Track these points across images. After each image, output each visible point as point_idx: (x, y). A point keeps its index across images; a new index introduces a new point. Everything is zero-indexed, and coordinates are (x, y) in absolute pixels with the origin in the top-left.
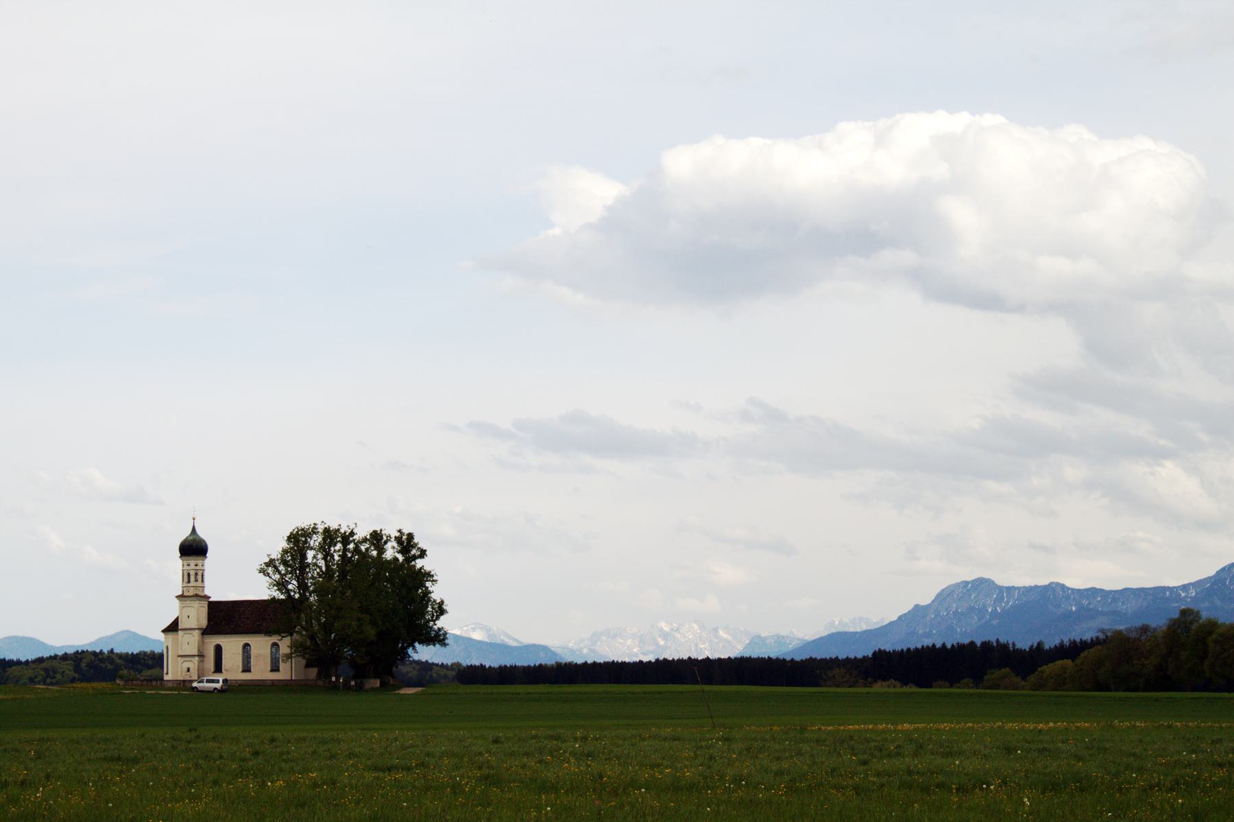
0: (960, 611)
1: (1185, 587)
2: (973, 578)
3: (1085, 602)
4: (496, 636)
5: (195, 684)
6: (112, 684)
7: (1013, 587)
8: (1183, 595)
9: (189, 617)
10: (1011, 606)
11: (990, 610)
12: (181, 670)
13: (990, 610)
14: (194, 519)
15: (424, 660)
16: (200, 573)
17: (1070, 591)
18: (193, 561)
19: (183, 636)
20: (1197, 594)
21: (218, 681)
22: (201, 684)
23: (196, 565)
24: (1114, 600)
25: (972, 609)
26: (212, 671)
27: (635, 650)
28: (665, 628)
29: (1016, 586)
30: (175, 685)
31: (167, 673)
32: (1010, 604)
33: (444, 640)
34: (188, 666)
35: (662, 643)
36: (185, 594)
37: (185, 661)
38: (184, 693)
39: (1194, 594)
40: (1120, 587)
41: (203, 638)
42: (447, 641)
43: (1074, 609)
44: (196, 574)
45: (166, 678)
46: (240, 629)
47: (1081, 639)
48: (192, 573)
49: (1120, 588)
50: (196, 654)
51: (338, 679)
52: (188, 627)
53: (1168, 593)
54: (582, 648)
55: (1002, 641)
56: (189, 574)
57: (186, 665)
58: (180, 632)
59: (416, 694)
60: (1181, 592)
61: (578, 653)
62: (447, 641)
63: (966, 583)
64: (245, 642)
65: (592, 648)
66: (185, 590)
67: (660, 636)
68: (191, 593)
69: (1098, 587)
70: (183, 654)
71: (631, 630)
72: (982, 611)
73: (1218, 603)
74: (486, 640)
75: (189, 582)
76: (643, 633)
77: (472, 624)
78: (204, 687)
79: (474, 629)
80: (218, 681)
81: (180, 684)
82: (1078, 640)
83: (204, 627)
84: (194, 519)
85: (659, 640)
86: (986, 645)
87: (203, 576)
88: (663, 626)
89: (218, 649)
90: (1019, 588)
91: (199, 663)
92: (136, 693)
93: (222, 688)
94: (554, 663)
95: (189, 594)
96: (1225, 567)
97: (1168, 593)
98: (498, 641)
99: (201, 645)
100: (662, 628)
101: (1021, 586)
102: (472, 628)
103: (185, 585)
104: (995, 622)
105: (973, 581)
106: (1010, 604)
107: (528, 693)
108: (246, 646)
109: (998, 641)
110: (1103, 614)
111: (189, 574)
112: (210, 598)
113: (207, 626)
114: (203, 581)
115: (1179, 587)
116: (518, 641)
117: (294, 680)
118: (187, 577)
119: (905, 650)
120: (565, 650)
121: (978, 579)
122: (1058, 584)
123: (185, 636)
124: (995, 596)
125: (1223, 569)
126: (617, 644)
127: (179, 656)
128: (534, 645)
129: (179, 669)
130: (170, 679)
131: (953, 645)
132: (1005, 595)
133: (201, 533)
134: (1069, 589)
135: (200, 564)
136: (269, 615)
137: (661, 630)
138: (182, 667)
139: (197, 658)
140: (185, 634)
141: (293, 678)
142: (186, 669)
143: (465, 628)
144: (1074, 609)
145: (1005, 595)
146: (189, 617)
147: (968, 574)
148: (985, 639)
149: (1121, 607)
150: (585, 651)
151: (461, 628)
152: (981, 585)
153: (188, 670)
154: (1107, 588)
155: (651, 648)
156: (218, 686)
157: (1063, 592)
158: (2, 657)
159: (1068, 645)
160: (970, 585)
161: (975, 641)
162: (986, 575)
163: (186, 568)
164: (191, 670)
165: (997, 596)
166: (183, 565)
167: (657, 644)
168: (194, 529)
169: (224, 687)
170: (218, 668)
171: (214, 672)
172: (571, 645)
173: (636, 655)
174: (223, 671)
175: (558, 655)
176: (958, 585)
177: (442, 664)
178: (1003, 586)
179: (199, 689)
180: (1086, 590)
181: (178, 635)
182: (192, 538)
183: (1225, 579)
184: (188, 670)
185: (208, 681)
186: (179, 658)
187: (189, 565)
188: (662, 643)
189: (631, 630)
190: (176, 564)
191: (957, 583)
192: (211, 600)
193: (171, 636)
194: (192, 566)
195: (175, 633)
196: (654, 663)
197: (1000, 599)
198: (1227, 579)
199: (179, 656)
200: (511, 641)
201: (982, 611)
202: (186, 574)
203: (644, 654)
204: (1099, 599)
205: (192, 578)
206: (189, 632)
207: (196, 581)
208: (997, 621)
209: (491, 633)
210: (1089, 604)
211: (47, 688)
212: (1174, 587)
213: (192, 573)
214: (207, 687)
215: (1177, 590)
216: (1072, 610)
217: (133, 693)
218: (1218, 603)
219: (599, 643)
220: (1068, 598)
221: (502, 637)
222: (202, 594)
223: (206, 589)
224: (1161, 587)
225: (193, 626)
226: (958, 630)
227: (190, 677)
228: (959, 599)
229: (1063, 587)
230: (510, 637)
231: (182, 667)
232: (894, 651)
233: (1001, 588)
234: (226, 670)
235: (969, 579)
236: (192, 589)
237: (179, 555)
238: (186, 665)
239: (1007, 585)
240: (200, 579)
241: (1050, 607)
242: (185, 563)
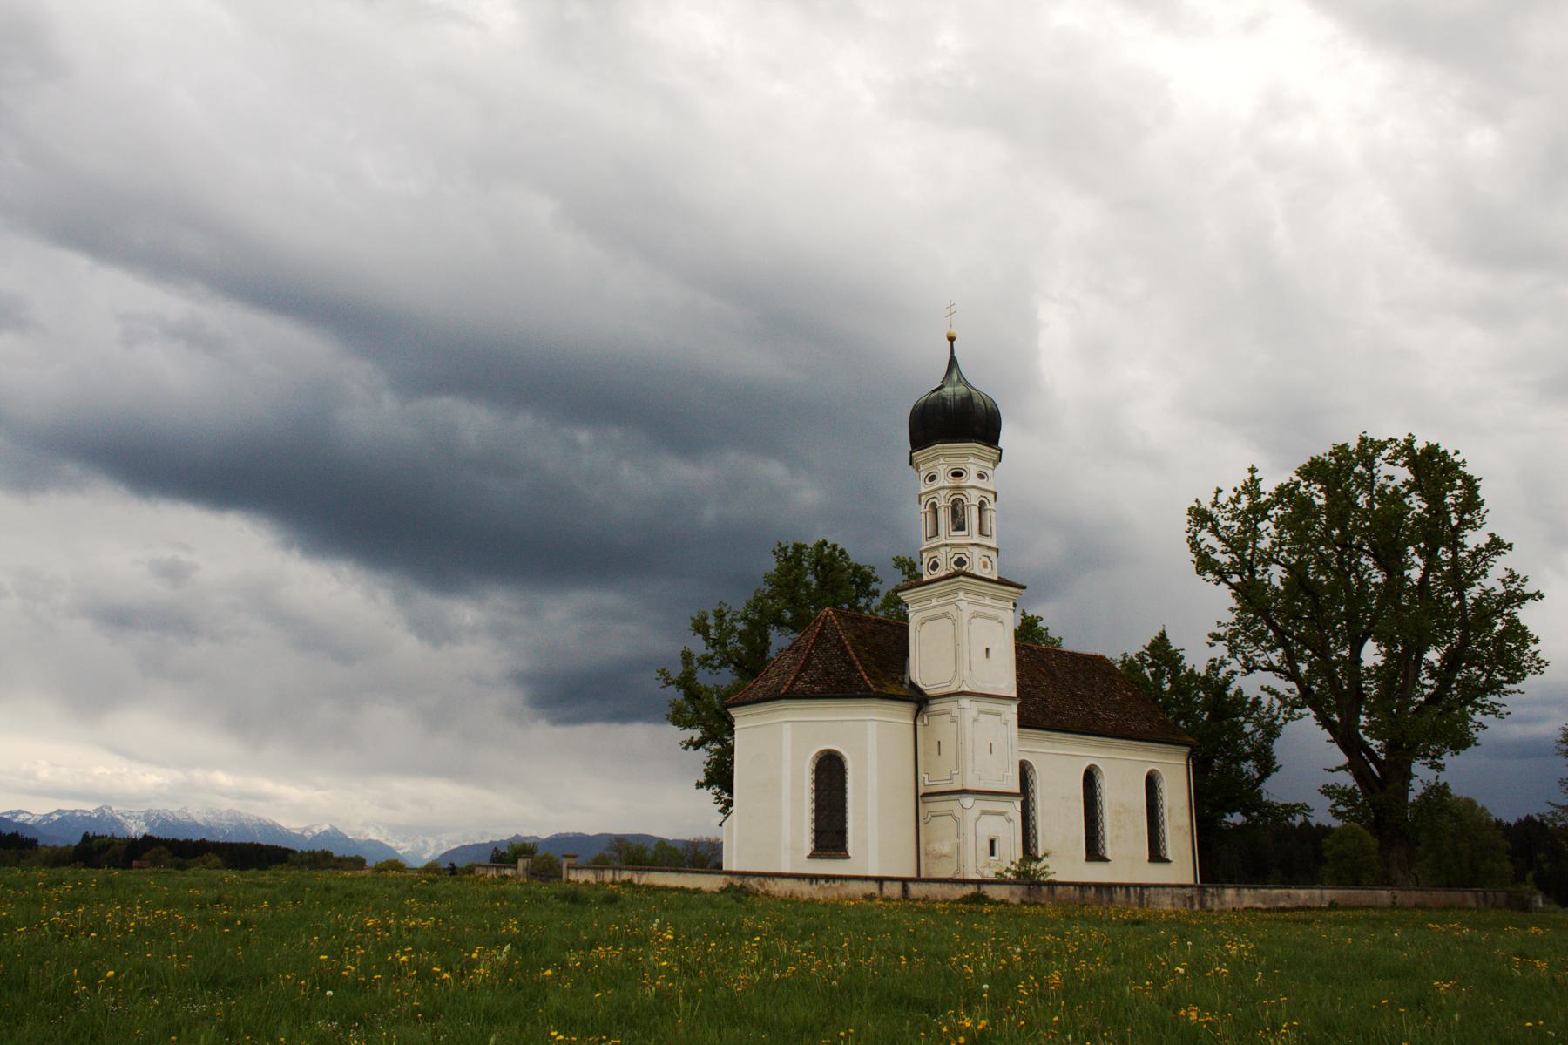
14: (952, 339)
56: (960, 526)
84: (952, 339)
95: (985, 573)
123: (982, 717)
171: (811, 856)
194: (944, 480)
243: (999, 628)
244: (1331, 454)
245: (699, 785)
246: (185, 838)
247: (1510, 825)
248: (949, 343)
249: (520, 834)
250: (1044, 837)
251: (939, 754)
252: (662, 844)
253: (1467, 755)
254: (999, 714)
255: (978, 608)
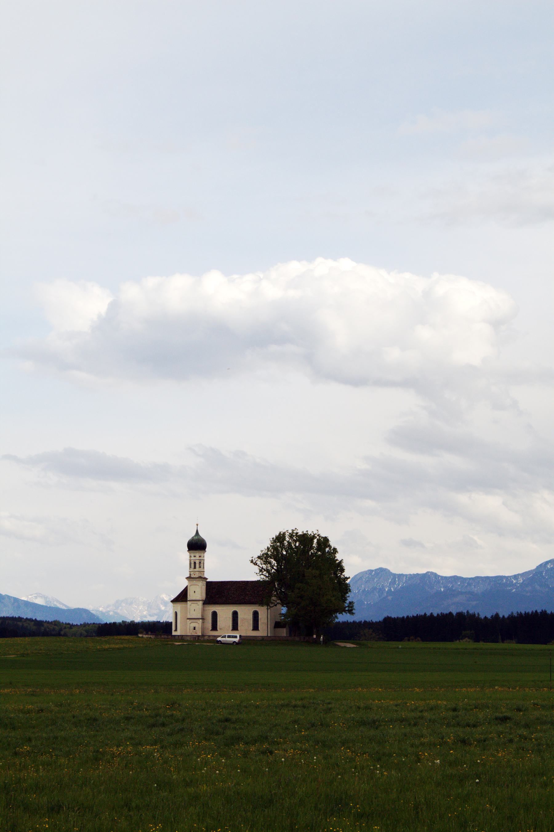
0: (366, 590)
1: (516, 577)
2: (376, 568)
3: (450, 585)
4: (51, 602)
5: (219, 639)
6: (137, 637)
7: (402, 574)
8: (514, 581)
9: (195, 592)
10: (401, 587)
11: (387, 590)
12: (190, 629)
13: (387, 590)
14: (197, 525)
15: (3, 616)
16: (202, 563)
17: (440, 578)
18: (197, 554)
19: (191, 605)
20: (524, 581)
21: (236, 637)
22: (224, 639)
23: (200, 557)
24: (469, 584)
25: (374, 589)
26: (210, 629)
27: (145, 613)
28: (165, 599)
29: (404, 573)
30: (192, 639)
31: (176, 630)
32: (400, 585)
33: (352, 610)
34: (194, 626)
35: (163, 608)
36: (192, 576)
37: (192, 622)
38: (204, 644)
39: (521, 581)
40: (473, 576)
41: (204, 607)
42: (354, 611)
43: (442, 590)
44: (200, 563)
45: (174, 633)
46: (230, 601)
47: (525, 612)
48: (197, 562)
49: (473, 576)
50: (200, 617)
51: (318, 637)
52: (194, 599)
53: (504, 580)
54: (109, 611)
55: (471, 612)
56: (195, 563)
57: (193, 625)
58: (188, 602)
59: (354, 647)
60: (513, 580)
61: (106, 614)
62: (354, 611)
63: (371, 571)
64: (213, 610)
65: (116, 611)
66: (192, 574)
67: (162, 604)
68: (197, 576)
69: (458, 575)
70: (191, 617)
71: (142, 599)
72: (381, 590)
73: (537, 587)
74: (44, 604)
75: (195, 568)
76: (150, 601)
77: (35, 594)
78: (226, 641)
79: (36, 597)
80: (236, 637)
81: (195, 638)
82: (523, 612)
83: (204, 599)
84: (197, 525)
85: (161, 606)
86: (460, 614)
87: (204, 564)
88: (164, 597)
89: (215, 615)
90: (406, 575)
91: (202, 624)
92: (184, 644)
93: (239, 641)
94: (121, 621)
95: (194, 576)
96: (543, 563)
97: (504, 580)
98: (52, 606)
99: (203, 610)
100: (163, 598)
101: (408, 573)
102: (35, 597)
103: (192, 570)
104: (390, 598)
105: (376, 570)
106: (400, 585)
107: (466, 649)
108: (235, 614)
109: (468, 612)
110: (461, 593)
111: (195, 563)
112: (207, 579)
113: (206, 598)
114: (204, 568)
115: (512, 576)
116: (66, 606)
117: (269, 637)
118: (193, 565)
119: (405, 617)
120: (98, 612)
121: (380, 568)
122: (432, 573)
123: (193, 605)
124: (390, 580)
125: (541, 565)
126: (133, 609)
127: (188, 619)
128: (78, 609)
129: (188, 627)
130: (179, 634)
131: (438, 614)
132: (397, 579)
133: (202, 535)
134: (439, 576)
135: (203, 556)
136: (249, 591)
137: (163, 600)
138: (190, 627)
139: (201, 620)
140: (192, 603)
141: (269, 635)
142: (193, 628)
143: (30, 597)
144: (442, 590)
145: (397, 579)
146: (195, 592)
147: (374, 566)
148: (459, 610)
149: (475, 589)
150: (111, 613)
151: (27, 596)
152: (381, 572)
153: (195, 628)
154: (464, 576)
155: (155, 612)
156: (237, 640)
157: (435, 578)
158: (1, 616)
159: (516, 615)
160: (374, 573)
161: (452, 611)
162: (384, 566)
163: (193, 558)
164: (196, 629)
165: (391, 581)
166: (191, 557)
167: (160, 609)
168: (197, 531)
169: (240, 641)
170: (235, 627)
171: (212, 630)
172: (101, 609)
173: (145, 616)
174: (218, 629)
175: (95, 616)
176: (366, 572)
177: (46, 621)
178: (395, 574)
179: (222, 642)
180: (451, 577)
181: (187, 604)
182: (196, 538)
183: (543, 571)
184: (195, 628)
185: (229, 637)
186: (188, 620)
187: (195, 556)
188: (163, 608)
189: (142, 599)
190: (185, 556)
191: (365, 571)
192: (208, 580)
193: (179, 606)
194: (197, 558)
195: (184, 603)
196: (18, 618)
197: (393, 582)
198: (544, 572)
199: (188, 619)
200: (61, 606)
201: (381, 590)
202: (192, 563)
203: (150, 615)
204: (459, 583)
205: (197, 566)
206: (195, 602)
207: (200, 567)
208: (392, 597)
209: (48, 600)
210: (452, 587)
211: (201, 644)
212: (508, 577)
213: (197, 562)
214: (228, 641)
215: (510, 578)
216: (441, 590)
217: (183, 644)
218: (537, 587)
219: (120, 608)
220: (439, 582)
221: (55, 603)
222: (203, 577)
223: (205, 573)
224: (500, 576)
225: (198, 598)
226: (365, 602)
227: (196, 633)
228: (366, 582)
229: (435, 575)
230: (61, 603)
231: (190, 627)
232: (398, 618)
233: (394, 575)
234: (220, 629)
235: (373, 569)
236: (197, 573)
237: (187, 549)
238: (193, 625)
239: (398, 573)
240: (202, 567)
241: (427, 588)
242: (192, 555)
243: (198, 586)
244: (259, 557)
245: (342, 560)
246: (383, 617)
247: (351, 622)
248: (197, 526)
249: (443, 612)
250: (219, 626)
251: (176, 613)
252: (39, 623)
253: (355, 604)
254: (197, 603)
255: (192, 584)
